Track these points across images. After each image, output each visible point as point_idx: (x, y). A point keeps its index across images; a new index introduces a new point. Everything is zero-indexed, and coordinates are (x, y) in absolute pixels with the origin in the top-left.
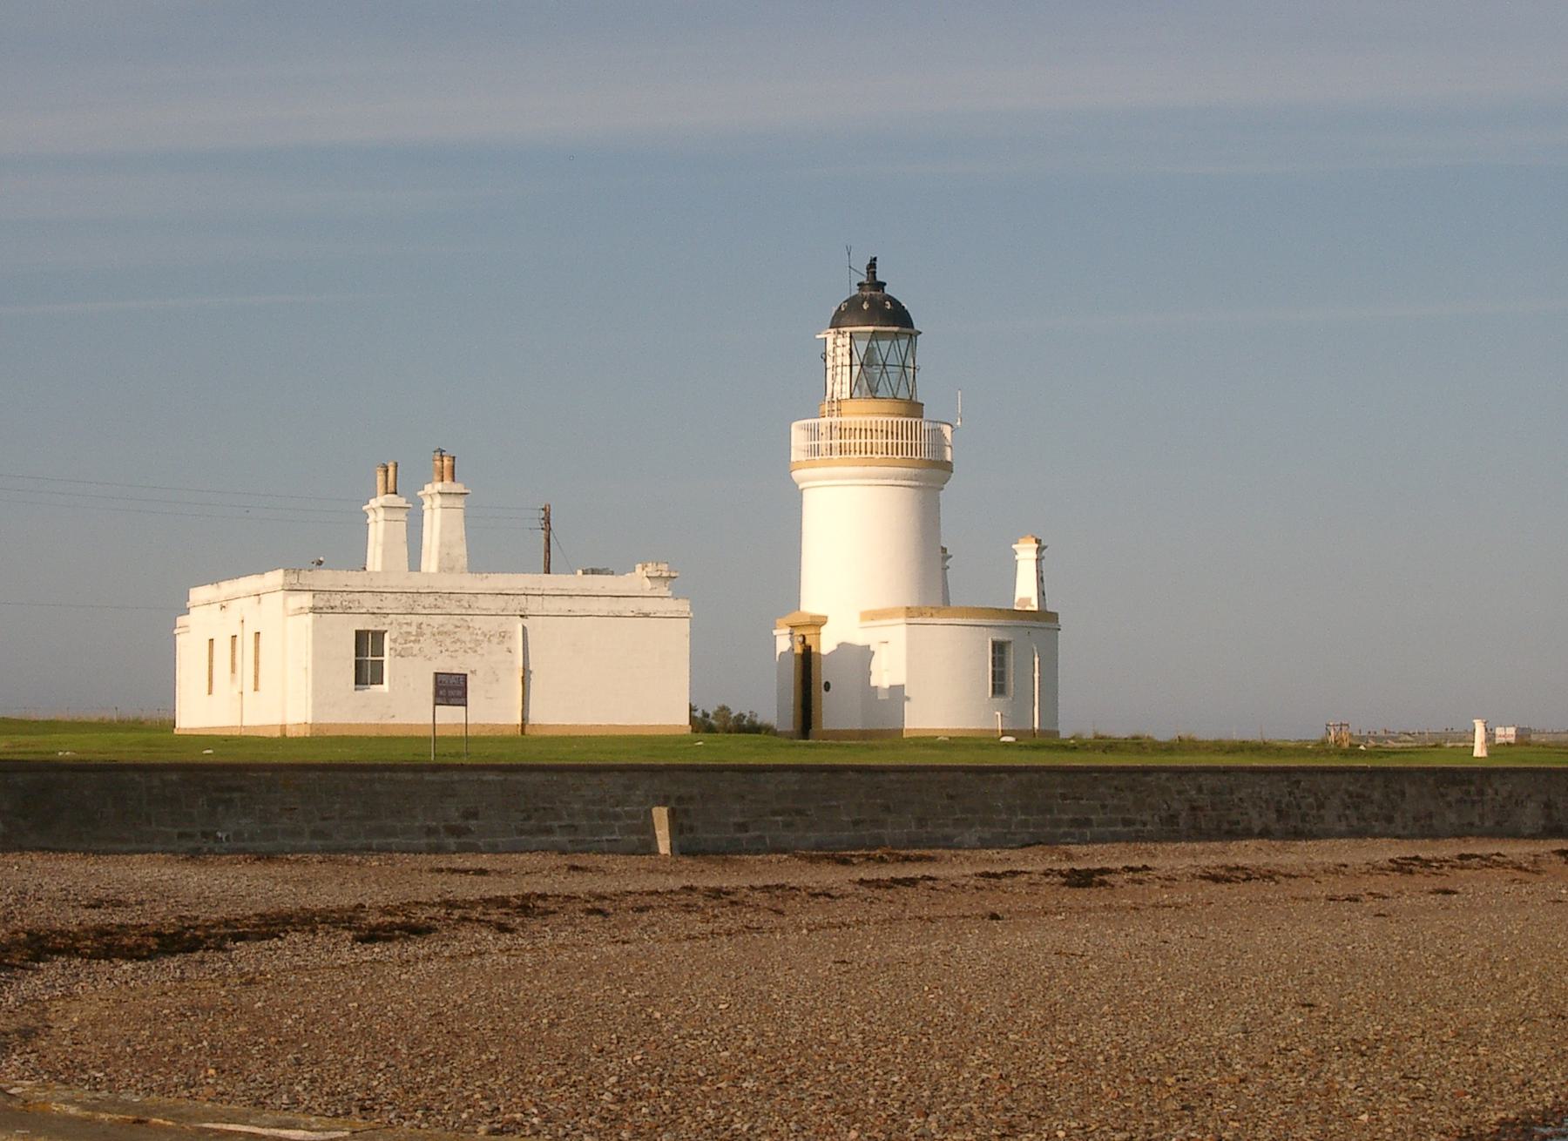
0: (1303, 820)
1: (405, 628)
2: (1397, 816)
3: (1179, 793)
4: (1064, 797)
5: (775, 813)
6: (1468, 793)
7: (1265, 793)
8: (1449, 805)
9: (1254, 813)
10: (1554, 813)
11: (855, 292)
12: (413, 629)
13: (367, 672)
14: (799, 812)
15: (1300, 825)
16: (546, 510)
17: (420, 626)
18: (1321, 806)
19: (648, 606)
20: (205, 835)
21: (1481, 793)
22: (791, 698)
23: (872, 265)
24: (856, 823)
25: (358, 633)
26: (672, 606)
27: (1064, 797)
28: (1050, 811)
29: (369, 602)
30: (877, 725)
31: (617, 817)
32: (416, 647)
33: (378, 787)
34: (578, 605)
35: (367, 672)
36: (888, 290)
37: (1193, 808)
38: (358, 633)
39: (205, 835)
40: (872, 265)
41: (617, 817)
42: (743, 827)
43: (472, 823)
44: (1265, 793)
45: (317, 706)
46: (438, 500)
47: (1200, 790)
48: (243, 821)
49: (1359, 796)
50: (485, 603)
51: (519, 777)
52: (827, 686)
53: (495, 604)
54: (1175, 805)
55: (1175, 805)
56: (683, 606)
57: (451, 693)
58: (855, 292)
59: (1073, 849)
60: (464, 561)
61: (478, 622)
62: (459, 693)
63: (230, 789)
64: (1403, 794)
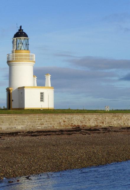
2: (104, 122)
4: (38, 120)
8: (115, 120)
9: (76, 122)
13: (42, 99)
15: (85, 124)
21: (121, 118)
28: (36, 122)
35: (42, 99)
37: (64, 121)
40: (21, 27)
45: (55, 105)
49: (97, 119)
52: (13, 101)
54: (60, 121)
55: (60, 121)
64: (106, 118)
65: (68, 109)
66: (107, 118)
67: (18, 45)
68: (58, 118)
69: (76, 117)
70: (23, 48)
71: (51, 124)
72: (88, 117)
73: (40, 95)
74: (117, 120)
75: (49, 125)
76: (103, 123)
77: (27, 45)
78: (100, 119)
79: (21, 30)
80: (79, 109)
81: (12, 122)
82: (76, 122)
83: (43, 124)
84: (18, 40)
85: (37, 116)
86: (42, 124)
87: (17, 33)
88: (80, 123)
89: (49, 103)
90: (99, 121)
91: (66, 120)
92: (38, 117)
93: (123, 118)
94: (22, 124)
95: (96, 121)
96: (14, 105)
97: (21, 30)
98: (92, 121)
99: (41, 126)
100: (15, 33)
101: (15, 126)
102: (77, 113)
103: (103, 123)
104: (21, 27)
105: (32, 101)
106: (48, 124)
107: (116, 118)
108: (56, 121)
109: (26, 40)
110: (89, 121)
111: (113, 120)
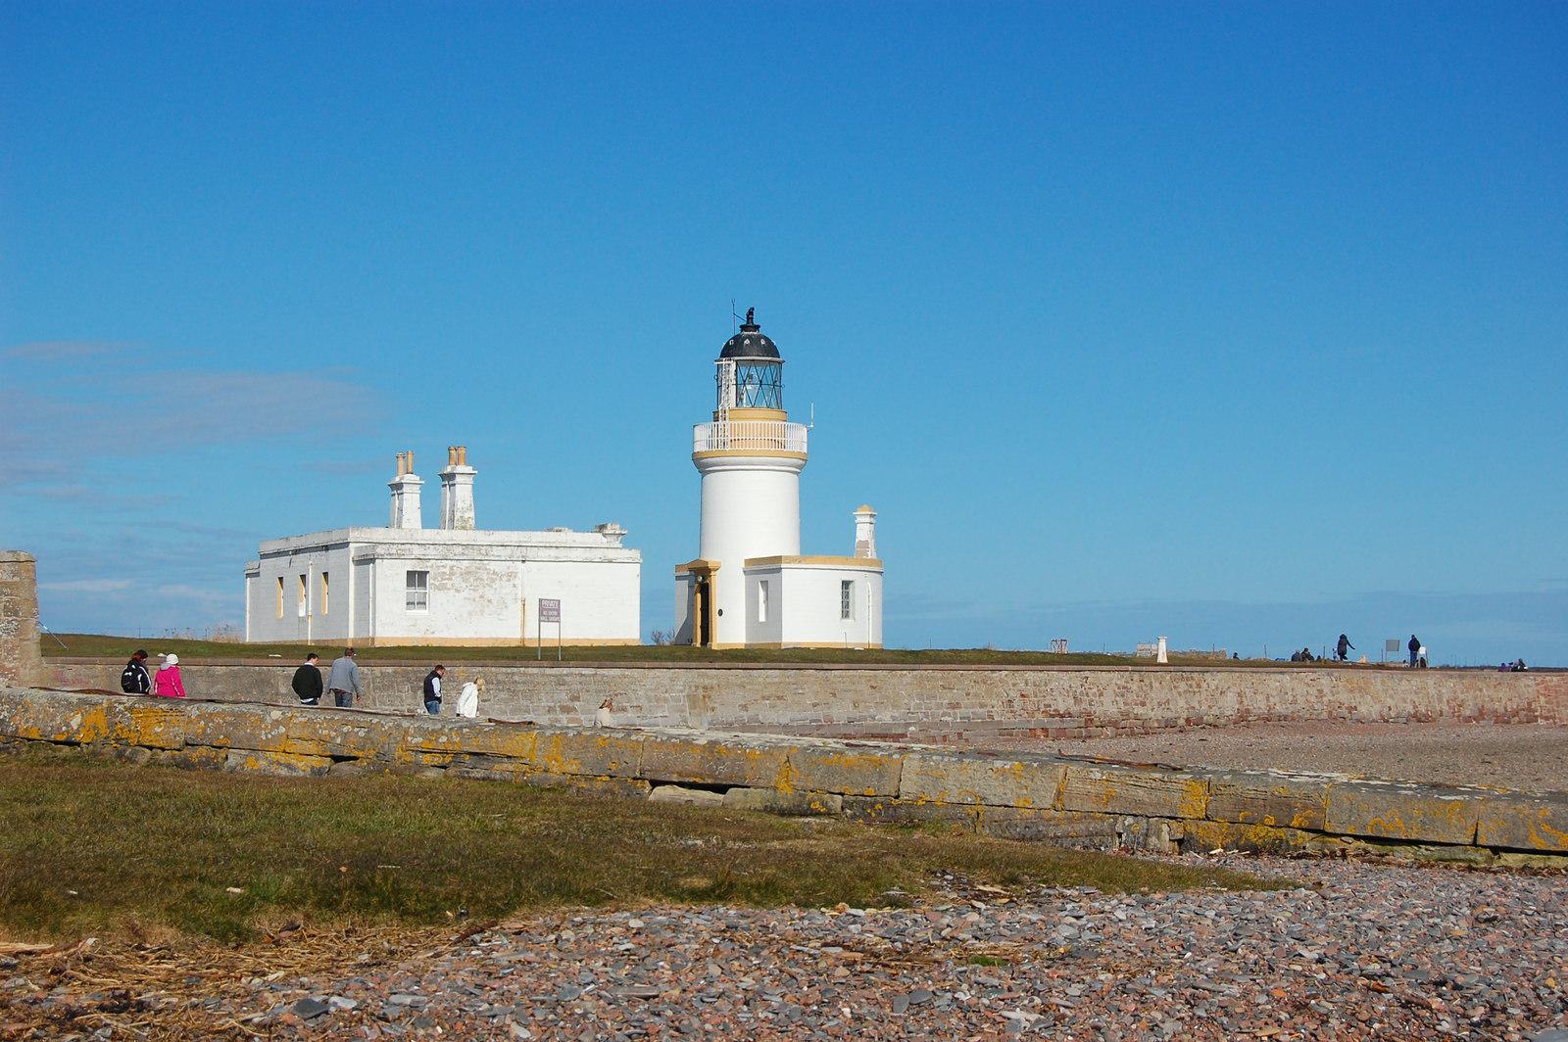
0: (1090, 705)
1: (442, 570)
3: (1014, 685)
6: (1191, 686)
9: (1060, 700)
10: (1244, 699)
11: (738, 331)
12: (447, 570)
14: (779, 698)
17: (452, 568)
18: (1101, 695)
19: (611, 554)
21: (1199, 686)
23: (751, 312)
24: (815, 705)
25: (843, 582)
26: (626, 554)
28: (935, 697)
29: (417, 551)
32: (449, 583)
33: (516, 678)
34: (562, 554)
36: (762, 331)
38: (843, 582)
40: (751, 312)
42: (745, 707)
43: (577, 704)
45: (887, 626)
49: (1124, 688)
50: (496, 551)
51: (74, 689)
52: (721, 613)
53: (504, 553)
54: (1012, 694)
55: (1012, 694)
56: (635, 554)
57: (550, 613)
58: (738, 331)
59: (284, 772)
60: (472, 522)
61: (492, 566)
62: (555, 613)
64: (1151, 687)
65: (981, 648)
66: (1156, 685)
71: (982, 706)
73: (1516, 661)
77: (776, 385)
79: (749, 325)
85: (837, 676)
86: (955, 706)
89: (863, 631)
90: (1131, 697)
91: (1030, 690)
93: (1204, 685)
95: (1123, 696)
97: (749, 325)
98: (1107, 700)
99: (951, 711)
102: (497, 658)
106: (973, 707)
107: (1182, 686)
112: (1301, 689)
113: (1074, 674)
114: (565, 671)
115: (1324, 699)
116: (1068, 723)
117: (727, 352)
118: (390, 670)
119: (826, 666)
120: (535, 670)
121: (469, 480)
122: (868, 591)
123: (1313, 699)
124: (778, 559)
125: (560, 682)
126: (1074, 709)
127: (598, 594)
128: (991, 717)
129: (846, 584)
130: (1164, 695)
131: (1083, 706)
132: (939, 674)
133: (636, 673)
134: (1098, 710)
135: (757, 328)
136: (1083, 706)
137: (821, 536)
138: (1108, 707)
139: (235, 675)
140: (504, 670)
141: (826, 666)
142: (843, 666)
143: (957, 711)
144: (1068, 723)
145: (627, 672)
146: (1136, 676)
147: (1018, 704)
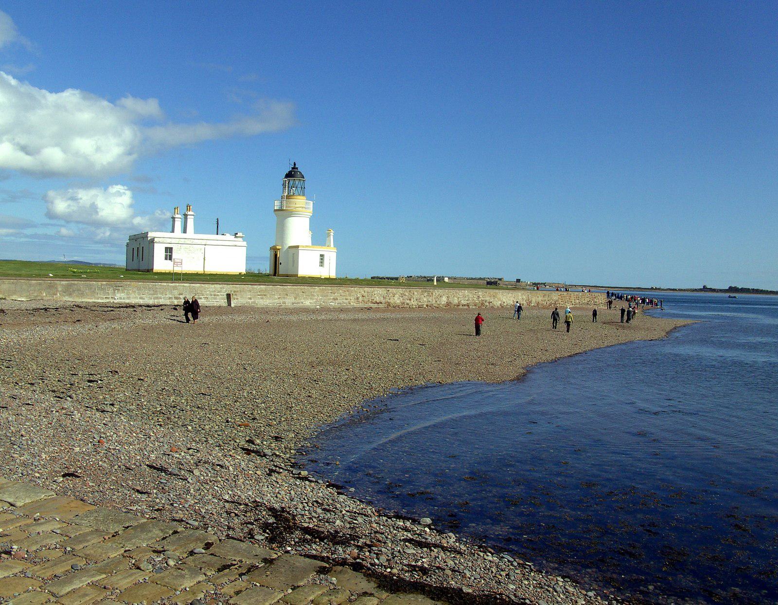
2: (412, 299)
4: (331, 293)
5: (258, 295)
7: (380, 293)
8: (424, 296)
9: (377, 298)
13: (322, 263)
15: (389, 301)
16: (217, 219)
20: (112, 298)
21: (432, 294)
22: (273, 268)
24: (279, 298)
25: (166, 248)
27: (331, 293)
29: (169, 241)
30: (289, 273)
31: (218, 295)
35: (322, 263)
37: (363, 296)
38: (166, 248)
39: (112, 298)
40: (295, 164)
41: (218, 295)
42: (250, 299)
44: (380, 293)
46: (188, 212)
47: (365, 292)
48: (122, 295)
54: (358, 295)
56: (245, 244)
57: (178, 264)
63: (119, 287)
64: (414, 294)
65: (354, 278)
66: (416, 293)
67: (290, 188)
68: (356, 291)
69: (377, 291)
70: (296, 193)
71: (346, 299)
72: (393, 292)
73: (319, 257)
74: (428, 297)
75: (345, 301)
76: (410, 300)
78: (407, 294)
80: (755, 288)
81: (298, 295)
82: (377, 298)
83: (337, 299)
84: (291, 182)
87: (290, 172)
88: (382, 298)
89: (329, 271)
91: (365, 294)
92: (331, 290)
93: (434, 294)
94: (311, 299)
96: (282, 270)
100: (287, 172)
101: (303, 300)
103: (410, 300)
104: (479, 314)
105: (308, 265)
107: (426, 294)
108: (353, 296)
109: (302, 182)
110: (394, 296)
111: (422, 296)
112: (471, 296)
113: (384, 289)
114: (177, 284)
115: (480, 299)
116: (381, 306)
117: (287, 176)
118: (104, 283)
119: (267, 284)
120: (165, 284)
121: (193, 220)
122: (331, 256)
123: (475, 299)
124: (298, 247)
125: (175, 288)
126: (383, 301)
127: (229, 256)
128: (349, 303)
129: (322, 256)
130: (418, 297)
131: (387, 300)
132: (330, 288)
133: (207, 286)
134: (392, 301)
135: (297, 168)
136: (387, 300)
137: (318, 239)
138: (397, 300)
139: (40, 284)
140: (152, 284)
141: (284, 284)
142: (291, 285)
143: (337, 301)
144: (381, 306)
145: (203, 285)
146: (408, 290)
147: (361, 299)
